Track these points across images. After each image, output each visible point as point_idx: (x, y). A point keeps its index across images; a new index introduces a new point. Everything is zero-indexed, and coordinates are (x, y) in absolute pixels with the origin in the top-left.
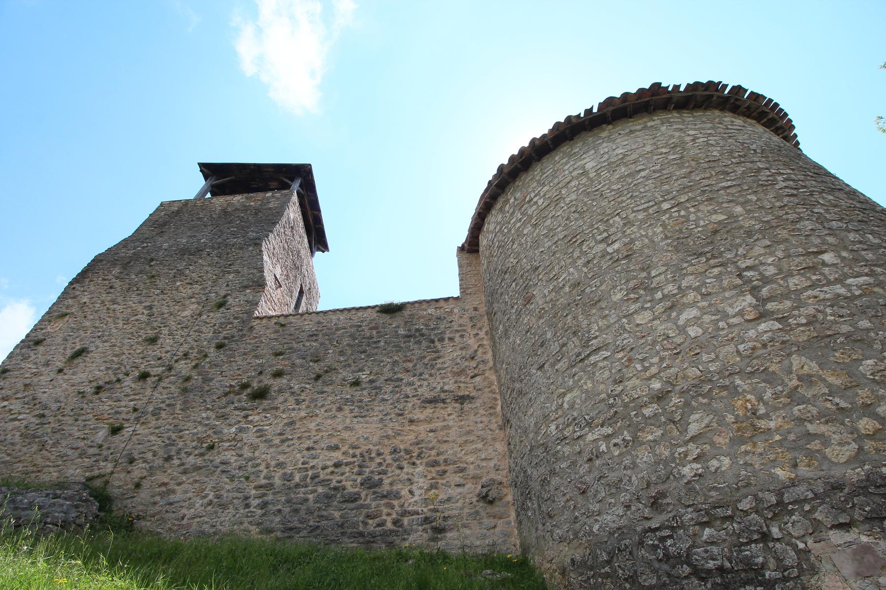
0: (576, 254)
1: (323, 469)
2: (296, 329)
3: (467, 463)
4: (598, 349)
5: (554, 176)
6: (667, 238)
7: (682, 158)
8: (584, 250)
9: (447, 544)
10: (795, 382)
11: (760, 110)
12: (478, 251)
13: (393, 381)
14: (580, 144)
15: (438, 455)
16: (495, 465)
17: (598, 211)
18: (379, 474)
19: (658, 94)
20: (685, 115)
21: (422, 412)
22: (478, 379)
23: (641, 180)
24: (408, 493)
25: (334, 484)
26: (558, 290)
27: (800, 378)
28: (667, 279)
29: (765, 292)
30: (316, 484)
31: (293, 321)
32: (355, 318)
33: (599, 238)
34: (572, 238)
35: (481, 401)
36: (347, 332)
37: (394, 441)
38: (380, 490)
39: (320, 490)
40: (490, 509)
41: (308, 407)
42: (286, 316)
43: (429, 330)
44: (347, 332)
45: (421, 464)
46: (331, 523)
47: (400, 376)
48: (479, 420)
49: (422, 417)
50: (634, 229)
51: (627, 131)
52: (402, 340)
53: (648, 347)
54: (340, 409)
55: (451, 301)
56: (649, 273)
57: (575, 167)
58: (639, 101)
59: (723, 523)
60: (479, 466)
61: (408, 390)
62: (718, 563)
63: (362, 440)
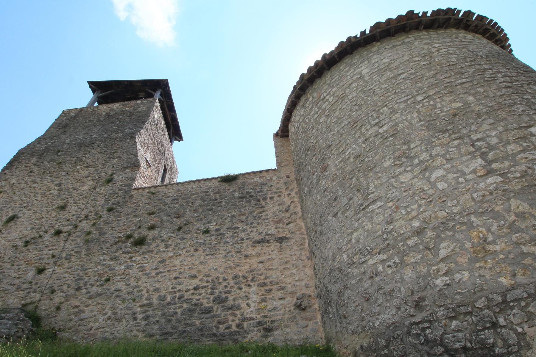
1: (186, 291)
2: (163, 196)
3: (286, 284)
5: (340, 80)
6: (421, 120)
7: (430, 64)
8: (363, 132)
10: (513, 218)
11: (484, 27)
12: (288, 136)
14: (357, 57)
15: (266, 278)
16: (306, 284)
17: (372, 103)
18: (226, 293)
19: (412, 19)
20: (431, 33)
21: (253, 250)
23: (402, 80)
25: (194, 301)
27: (516, 215)
28: (421, 150)
29: (491, 156)
30: (182, 302)
34: (354, 124)
35: (294, 240)
36: (198, 197)
37: (235, 270)
39: (185, 306)
42: (155, 187)
43: (256, 192)
45: (254, 285)
46: (193, 328)
47: (237, 225)
49: (253, 253)
50: (398, 115)
51: (391, 46)
53: (410, 198)
54: (196, 250)
55: (270, 171)
56: (409, 146)
57: (355, 73)
58: (399, 24)
60: (294, 285)
61: (243, 235)
63: (212, 270)
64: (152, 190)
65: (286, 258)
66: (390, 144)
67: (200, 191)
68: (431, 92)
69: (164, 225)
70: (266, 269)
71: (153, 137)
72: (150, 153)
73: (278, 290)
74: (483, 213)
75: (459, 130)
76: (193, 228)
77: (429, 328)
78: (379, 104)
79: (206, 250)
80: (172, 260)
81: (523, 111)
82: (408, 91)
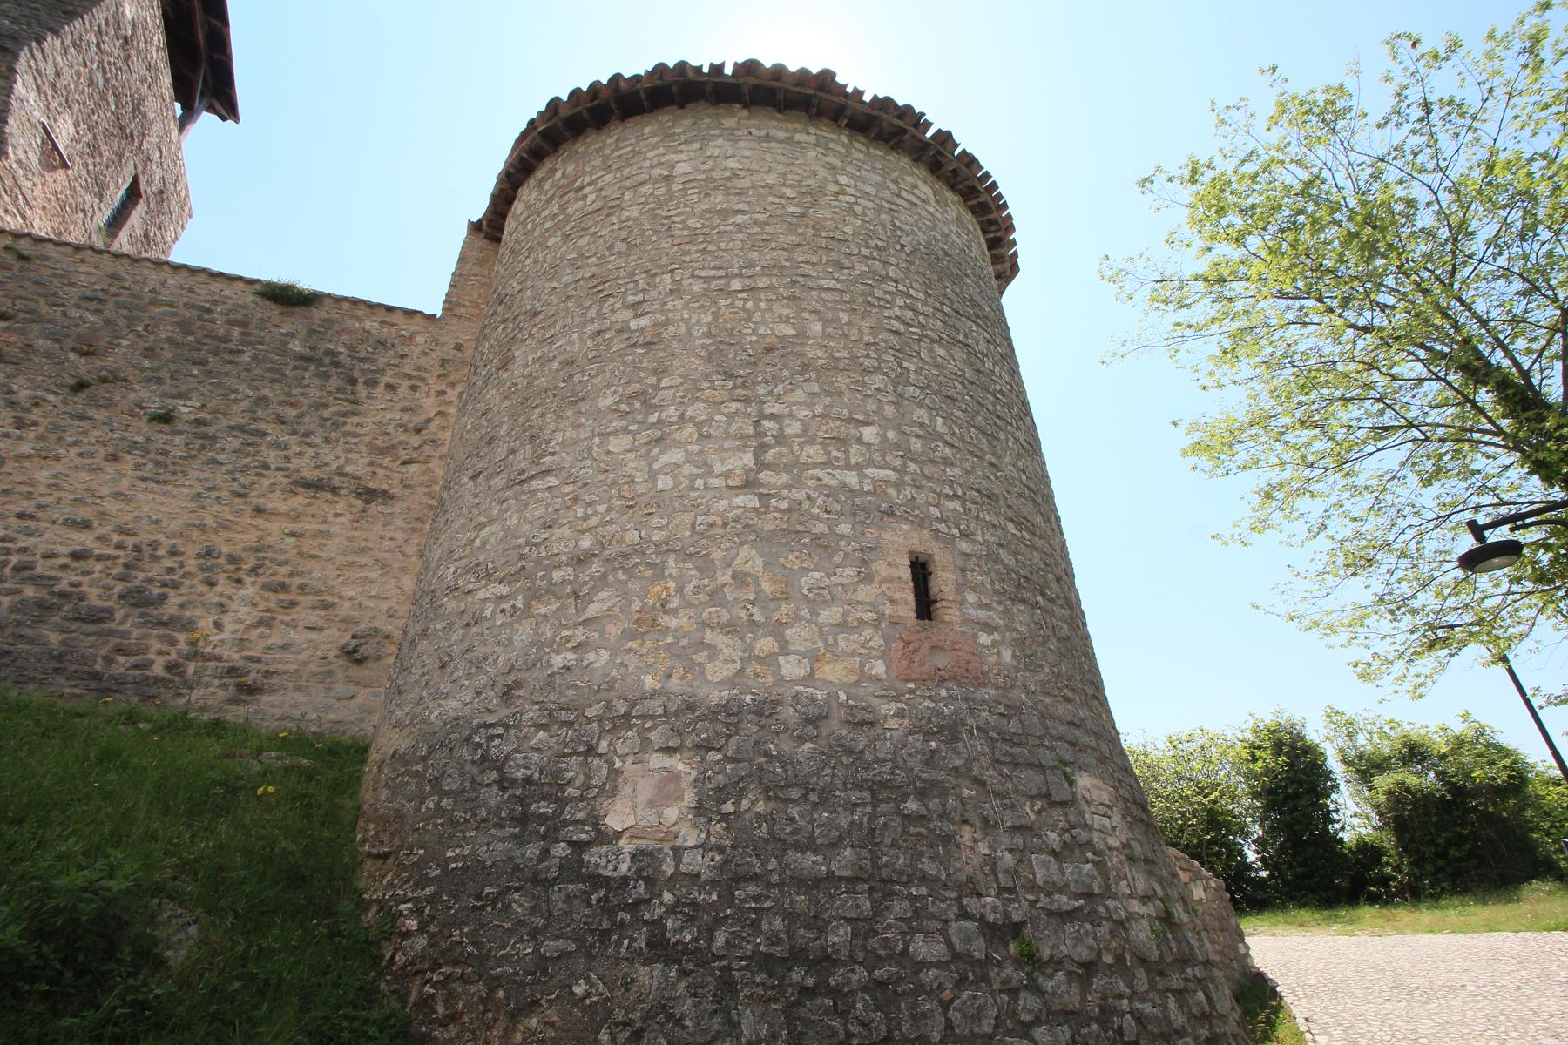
0: (592, 313)
1: (45, 557)
2: (55, 275)
3: (340, 598)
4: (548, 472)
5: (628, 162)
6: (709, 335)
7: (803, 215)
8: (605, 311)
9: (257, 712)
10: (727, 578)
11: (969, 183)
12: (498, 240)
13: (244, 432)
14: (687, 122)
15: (291, 575)
16: (390, 609)
17: (652, 253)
18: (164, 585)
19: (828, 92)
20: (857, 145)
21: (285, 500)
22: (413, 468)
23: (731, 228)
24: (211, 625)
25: (63, 586)
26: (544, 361)
27: (734, 576)
28: (674, 397)
29: (769, 456)
30: (23, 581)
31: (51, 254)
32: (203, 291)
33: (631, 299)
34: (599, 284)
35: (404, 505)
36: (174, 315)
37: (213, 537)
38: (156, 612)
39: (30, 592)
40: (355, 671)
41: (42, 438)
42: (38, 240)
43: (353, 358)
44: (174, 315)
45: (253, 583)
46: (36, 649)
47: (263, 426)
48: (388, 535)
49: (283, 507)
50: (679, 304)
51: (763, 133)
52: (292, 363)
53: (605, 488)
54: (114, 458)
55: (418, 318)
56: (659, 381)
57: (663, 160)
58: (797, 89)
59: (559, 729)
60: (360, 605)
61: (272, 457)
62: (528, 772)
63: (145, 522)
64: (24, 246)
65: (366, 540)
66: (633, 361)
67: (185, 300)
68: (762, 283)
69: (30, 360)
70: (301, 554)
71: (99, 77)
72: (76, 124)
73: (314, 608)
74: (691, 555)
75: (755, 384)
76: (123, 397)
77: (500, 736)
78: (664, 261)
79: (145, 465)
80: (27, 464)
81: (878, 389)
82: (728, 257)
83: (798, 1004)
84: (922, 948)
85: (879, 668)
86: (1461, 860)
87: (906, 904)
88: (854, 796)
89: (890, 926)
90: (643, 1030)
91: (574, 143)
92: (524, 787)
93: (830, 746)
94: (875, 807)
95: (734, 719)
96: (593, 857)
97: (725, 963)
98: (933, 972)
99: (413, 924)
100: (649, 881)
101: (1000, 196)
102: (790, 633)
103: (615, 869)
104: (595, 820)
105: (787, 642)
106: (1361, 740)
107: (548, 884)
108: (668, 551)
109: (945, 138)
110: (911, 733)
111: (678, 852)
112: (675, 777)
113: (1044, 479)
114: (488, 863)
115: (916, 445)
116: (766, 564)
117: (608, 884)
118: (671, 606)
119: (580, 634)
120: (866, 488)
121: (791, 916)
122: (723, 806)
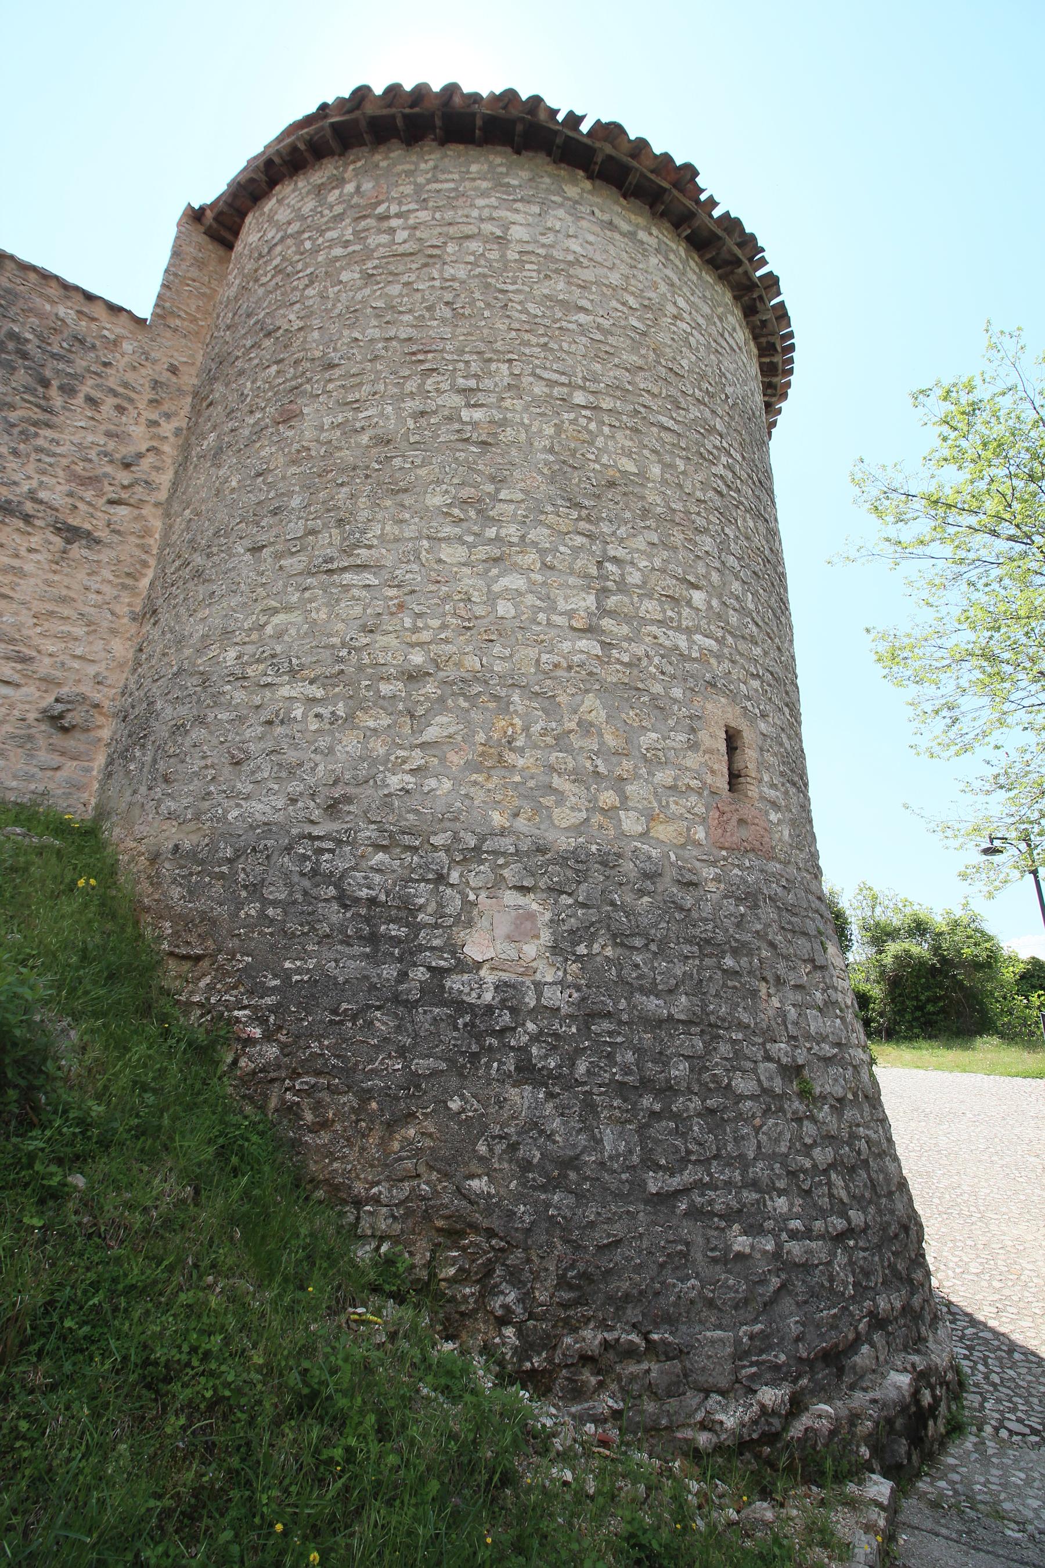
0: (411, 386)
3: (39, 652)
4: (364, 567)
6: (551, 451)
7: (644, 334)
10: (573, 725)
11: (772, 339)
12: (230, 246)
14: (525, 175)
16: (97, 674)
17: (486, 331)
19: (682, 191)
22: (122, 511)
26: (350, 430)
28: (515, 515)
29: (612, 601)
33: (461, 381)
35: (113, 554)
40: (58, 739)
43: (45, 351)
51: (606, 217)
55: (123, 318)
56: (498, 491)
57: (495, 215)
58: (653, 177)
60: (63, 664)
62: (373, 893)
65: (67, 587)
66: (466, 460)
74: (537, 694)
75: (600, 519)
82: (570, 362)
83: (647, 1126)
84: (743, 1085)
85: (700, 834)
86: (934, 1013)
87: (728, 1046)
88: (686, 949)
89: (717, 1063)
90: (518, 1144)
91: (373, 151)
92: (369, 908)
93: (665, 902)
94: (702, 960)
95: (580, 867)
96: (455, 983)
97: (587, 1088)
98: (749, 1104)
99: (257, 1032)
100: (513, 1010)
101: (791, 361)
102: (630, 789)
103: (479, 997)
104: (453, 949)
105: (627, 798)
106: (878, 910)
107: (411, 1005)
108: (513, 685)
109: (772, 282)
110: (726, 897)
111: (538, 986)
112: (531, 916)
113: (789, 666)
114: (341, 979)
115: (734, 618)
116: (608, 717)
117: (472, 1010)
118: (518, 744)
119: (417, 759)
120: (695, 655)
121: (638, 1050)
122: (577, 948)
